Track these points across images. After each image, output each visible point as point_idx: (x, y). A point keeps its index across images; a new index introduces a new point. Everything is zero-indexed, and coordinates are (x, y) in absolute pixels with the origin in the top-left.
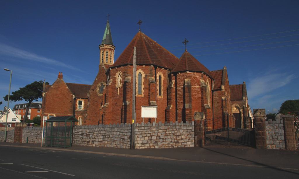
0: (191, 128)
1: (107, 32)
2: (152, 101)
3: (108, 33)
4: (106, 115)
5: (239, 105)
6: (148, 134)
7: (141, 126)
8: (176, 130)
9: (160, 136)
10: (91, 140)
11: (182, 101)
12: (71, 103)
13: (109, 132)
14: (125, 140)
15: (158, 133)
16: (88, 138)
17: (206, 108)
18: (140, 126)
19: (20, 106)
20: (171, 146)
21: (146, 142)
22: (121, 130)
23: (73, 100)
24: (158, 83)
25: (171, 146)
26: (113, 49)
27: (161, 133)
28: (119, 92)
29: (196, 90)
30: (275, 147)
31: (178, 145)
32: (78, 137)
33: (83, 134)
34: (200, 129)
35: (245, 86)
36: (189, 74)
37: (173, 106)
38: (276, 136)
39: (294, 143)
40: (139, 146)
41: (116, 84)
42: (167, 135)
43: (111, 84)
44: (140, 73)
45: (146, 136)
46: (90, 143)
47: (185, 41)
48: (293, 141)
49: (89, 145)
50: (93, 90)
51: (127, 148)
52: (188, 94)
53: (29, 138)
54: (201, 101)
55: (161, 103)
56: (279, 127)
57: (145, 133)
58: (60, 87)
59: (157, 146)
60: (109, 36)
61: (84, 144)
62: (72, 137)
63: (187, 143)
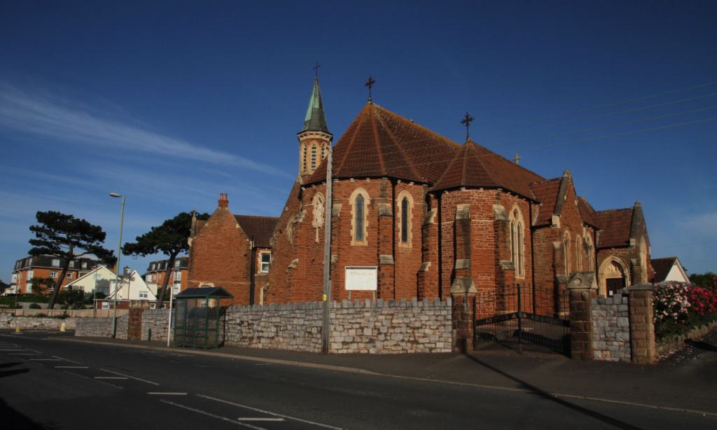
0: (444, 313)
1: (314, 103)
2: (384, 253)
3: (317, 106)
4: (294, 285)
5: (620, 260)
6: (357, 323)
7: (342, 308)
8: (414, 316)
9: (379, 329)
10: (256, 334)
11: (451, 253)
12: (246, 258)
13: (286, 319)
14: (312, 335)
15: (375, 322)
16: (251, 331)
17: (503, 268)
18: (340, 307)
19: (159, 265)
20: (403, 349)
21: (351, 340)
22: (307, 315)
23: (250, 252)
24: (399, 215)
25: (403, 349)
26: (328, 139)
27: (382, 322)
28: (319, 237)
29: (483, 230)
30: (611, 356)
31: (417, 348)
32: (234, 328)
33: (242, 322)
34: (464, 315)
35: (641, 211)
36: (466, 193)
37: (432, 264)
38: (612, 331)
39: (647, 347)
40: (337, 347)
41: (312, 219)
42: (394, 327)
43: (304, 220)
44: (360, 195)
45: (352, 328)
46: (254, 341)
47: (467, 117)
48: (645, 345)
49: (253, 346)
50: (281, 232)
51: (316, 351)
52: (462, 239)
53: (153, 330)
54: (495, 252)
55: (408, 258)
56: (618, 312)
57: (350, 321)
58: (222, 226)
59: (374, 349)
60: (320, 113)
61: (244, 343)
62: (224, 329)
63: (435, 344)
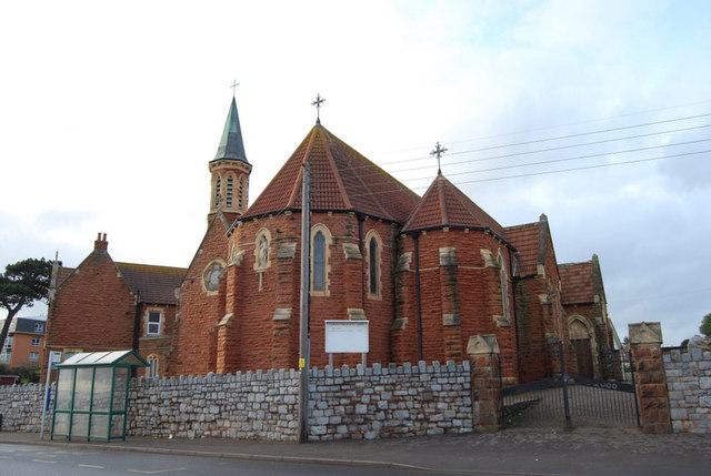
0: (460, 380)
40: (318, 432)
42: (397, 402)
